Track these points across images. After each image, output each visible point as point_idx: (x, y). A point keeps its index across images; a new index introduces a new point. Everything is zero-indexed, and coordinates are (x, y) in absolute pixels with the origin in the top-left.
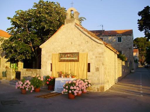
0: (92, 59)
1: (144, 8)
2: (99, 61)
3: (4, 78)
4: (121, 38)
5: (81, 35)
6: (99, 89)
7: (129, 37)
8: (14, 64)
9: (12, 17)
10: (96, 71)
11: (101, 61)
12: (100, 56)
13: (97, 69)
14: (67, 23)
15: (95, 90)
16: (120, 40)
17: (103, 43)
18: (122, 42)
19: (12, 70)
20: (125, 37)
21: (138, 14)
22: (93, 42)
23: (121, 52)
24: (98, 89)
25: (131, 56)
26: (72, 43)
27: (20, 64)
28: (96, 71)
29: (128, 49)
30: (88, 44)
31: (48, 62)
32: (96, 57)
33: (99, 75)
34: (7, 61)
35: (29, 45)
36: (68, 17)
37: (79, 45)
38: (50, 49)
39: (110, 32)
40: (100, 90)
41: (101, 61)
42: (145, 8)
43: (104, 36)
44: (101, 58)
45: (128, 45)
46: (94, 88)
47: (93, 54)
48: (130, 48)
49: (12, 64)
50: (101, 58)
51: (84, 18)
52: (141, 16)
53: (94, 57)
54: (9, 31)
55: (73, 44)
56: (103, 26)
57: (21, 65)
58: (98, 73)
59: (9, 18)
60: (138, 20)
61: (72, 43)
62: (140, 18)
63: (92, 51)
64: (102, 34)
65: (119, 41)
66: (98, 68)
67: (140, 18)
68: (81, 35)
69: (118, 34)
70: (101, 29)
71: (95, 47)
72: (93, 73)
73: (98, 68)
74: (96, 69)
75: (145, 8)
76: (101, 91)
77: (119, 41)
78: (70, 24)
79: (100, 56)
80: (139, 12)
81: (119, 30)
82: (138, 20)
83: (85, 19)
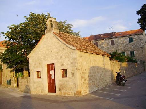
0: (68, 65)
1: (141, 7)
2: (74, 67)
3: (10, 87)
4: (132, 38)
5: (58, 43)
6: (76, 94)
7: (140, 36)
8: (20, 73)
9: (6, 32)
10: (72, 76)
11: (76, 66)
12: (74, 61)
13: (73, 75)
14: (47, 33)
15: (72, 95)
16: (131, 40)
17: (76, 49)
18: (133, 42)
19: (14, 79)
20: (135, 37)
21: (137, 13)
22: (68, 48)
23: (134, 52)
24: (74, 93)
25: (144, 56)
26: (51, 51)
27: (25, 72)
28: (72, 76)
29: (141, 49)
30: (64, 51)
31: (34, 70)
32: (71, 63)
33: (74, 80)
34: (11, 71)
35: (24, 55)
36: (49, 27)
37: (57, 53)
38: (39, 57)
39: (121, 34)
40: (77, 95)
41: (76, 66)
42: (142, 6)
43: (115, 38)
44: (75, 63)
45: (140, 44)
46: (71, 92)
47: (69, 60)
48: (142, 48)
49: (18, 73)
50: (75, 63)
51: (71, 25)
52: (140, 15)
53: (69, 63)
54: (5, 44)
55: (52, 52)
56: (113, 28)
57: (26, 73)
58: (74, 78)
59: (3, 33)
60: (139, 20)
61: (51, 51)
62: (139, 17)
63: (68, 57)
64: (113, 36)
65: (130, 42)
66: (73, 73)
67: (139, 17)
68: (58, 43)
69: (129, 34)
70: (112, 32)
71: (70, 54)
72: (70, 79)
73: (73, 73)
74: (72, 74)
75: (142, 6)
76: (77, 96)
77: (130, 42)
78: (49, 33)
79: (74, 61)
80: (137, 11)
81: (131, 31)
82: (139, 20)
83: (72, 25)
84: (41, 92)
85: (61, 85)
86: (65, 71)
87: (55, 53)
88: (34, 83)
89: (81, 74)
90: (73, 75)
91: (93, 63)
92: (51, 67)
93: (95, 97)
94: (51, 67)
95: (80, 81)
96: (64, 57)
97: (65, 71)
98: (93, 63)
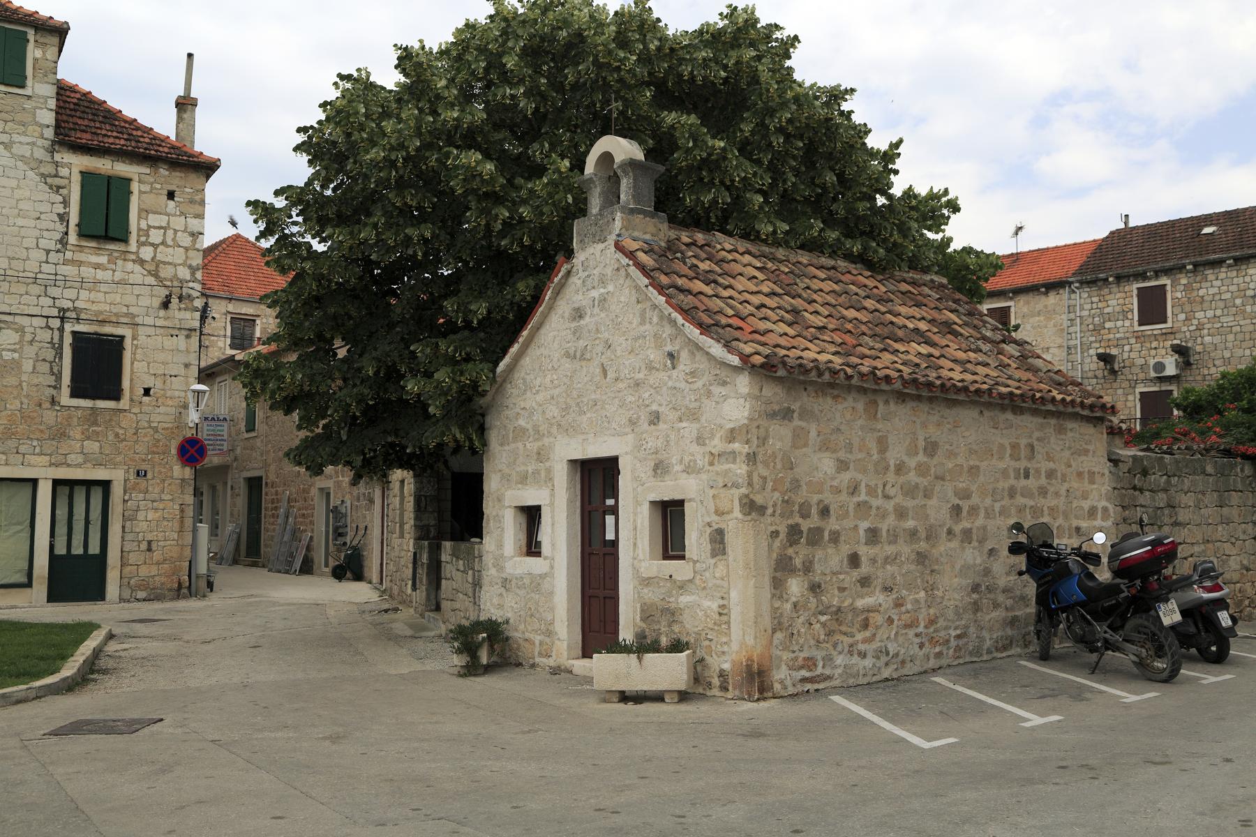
10: (714, 555)
13: (718, 540)
18: (1169, 324)
28: (714, 555)
47: (700, 440)
52: (788, 63)
55: (611, 375)
73: (720, 532)
74: (712, 541)
84: (540, 654)
85: (648, 614)
86: (670, 514)
87: (621, 385)
88: (505, 583)
89: (777, 543)
90: (718, 540)
91: (912, 463)
92: (598, 478)
93: (1100, 682)
94: (598, 478)
95: (767, 593)
96: (669, 415)
97: (670, 514)
98: (912, 463)
